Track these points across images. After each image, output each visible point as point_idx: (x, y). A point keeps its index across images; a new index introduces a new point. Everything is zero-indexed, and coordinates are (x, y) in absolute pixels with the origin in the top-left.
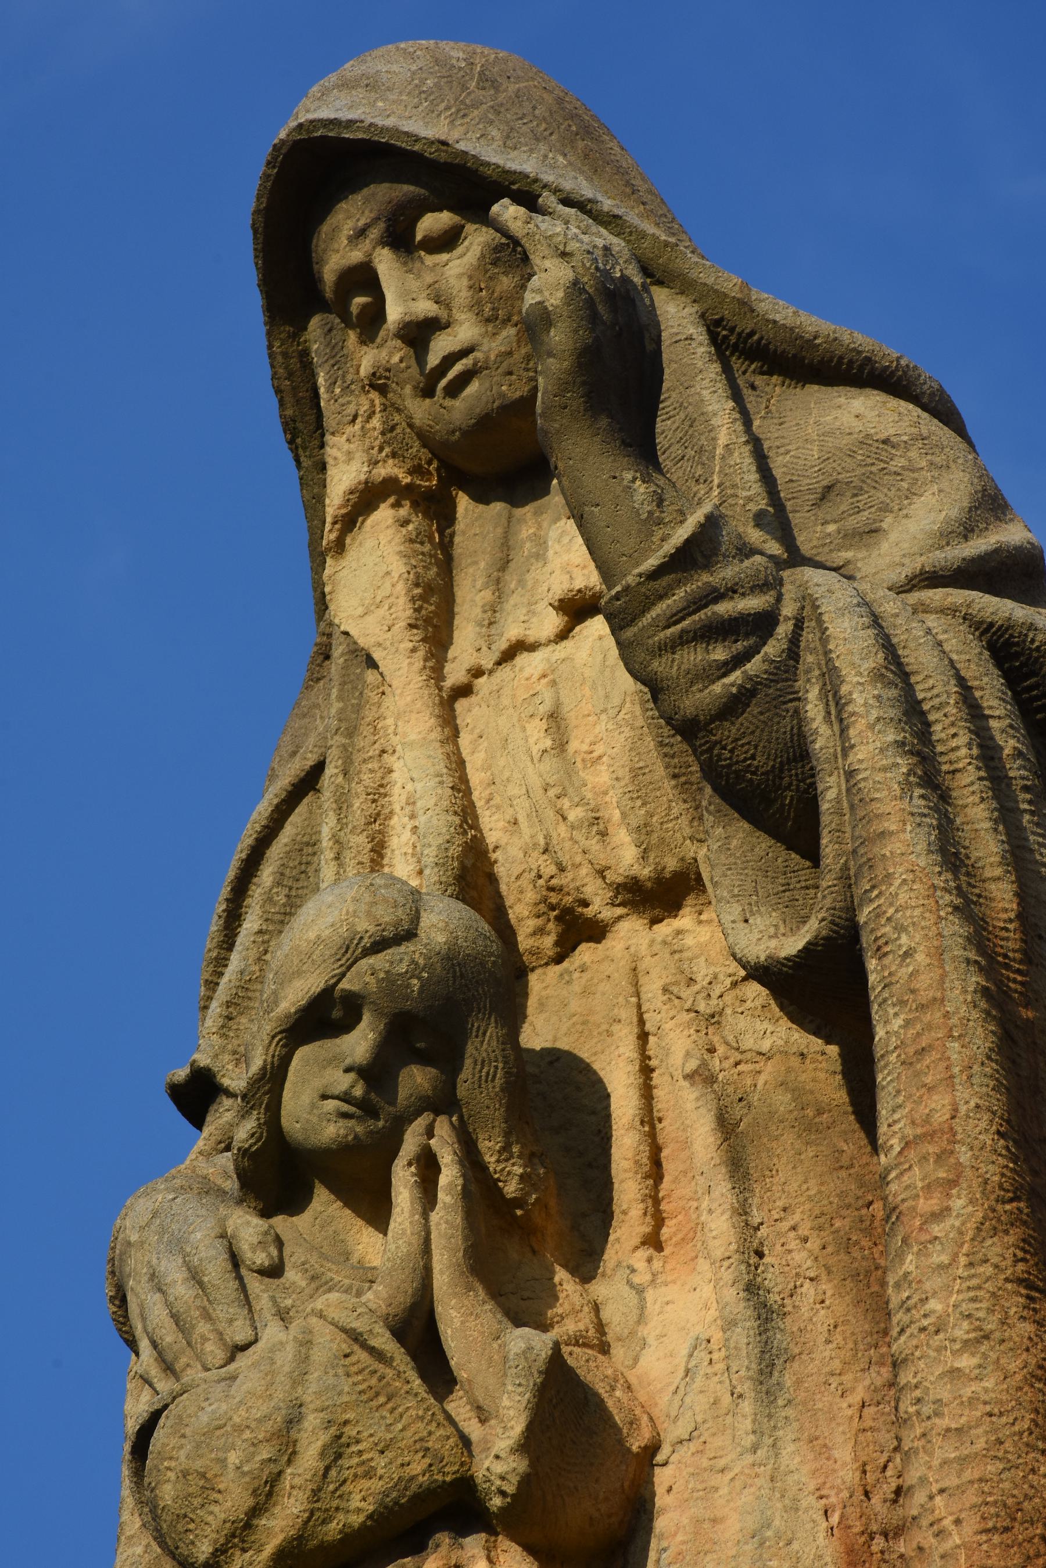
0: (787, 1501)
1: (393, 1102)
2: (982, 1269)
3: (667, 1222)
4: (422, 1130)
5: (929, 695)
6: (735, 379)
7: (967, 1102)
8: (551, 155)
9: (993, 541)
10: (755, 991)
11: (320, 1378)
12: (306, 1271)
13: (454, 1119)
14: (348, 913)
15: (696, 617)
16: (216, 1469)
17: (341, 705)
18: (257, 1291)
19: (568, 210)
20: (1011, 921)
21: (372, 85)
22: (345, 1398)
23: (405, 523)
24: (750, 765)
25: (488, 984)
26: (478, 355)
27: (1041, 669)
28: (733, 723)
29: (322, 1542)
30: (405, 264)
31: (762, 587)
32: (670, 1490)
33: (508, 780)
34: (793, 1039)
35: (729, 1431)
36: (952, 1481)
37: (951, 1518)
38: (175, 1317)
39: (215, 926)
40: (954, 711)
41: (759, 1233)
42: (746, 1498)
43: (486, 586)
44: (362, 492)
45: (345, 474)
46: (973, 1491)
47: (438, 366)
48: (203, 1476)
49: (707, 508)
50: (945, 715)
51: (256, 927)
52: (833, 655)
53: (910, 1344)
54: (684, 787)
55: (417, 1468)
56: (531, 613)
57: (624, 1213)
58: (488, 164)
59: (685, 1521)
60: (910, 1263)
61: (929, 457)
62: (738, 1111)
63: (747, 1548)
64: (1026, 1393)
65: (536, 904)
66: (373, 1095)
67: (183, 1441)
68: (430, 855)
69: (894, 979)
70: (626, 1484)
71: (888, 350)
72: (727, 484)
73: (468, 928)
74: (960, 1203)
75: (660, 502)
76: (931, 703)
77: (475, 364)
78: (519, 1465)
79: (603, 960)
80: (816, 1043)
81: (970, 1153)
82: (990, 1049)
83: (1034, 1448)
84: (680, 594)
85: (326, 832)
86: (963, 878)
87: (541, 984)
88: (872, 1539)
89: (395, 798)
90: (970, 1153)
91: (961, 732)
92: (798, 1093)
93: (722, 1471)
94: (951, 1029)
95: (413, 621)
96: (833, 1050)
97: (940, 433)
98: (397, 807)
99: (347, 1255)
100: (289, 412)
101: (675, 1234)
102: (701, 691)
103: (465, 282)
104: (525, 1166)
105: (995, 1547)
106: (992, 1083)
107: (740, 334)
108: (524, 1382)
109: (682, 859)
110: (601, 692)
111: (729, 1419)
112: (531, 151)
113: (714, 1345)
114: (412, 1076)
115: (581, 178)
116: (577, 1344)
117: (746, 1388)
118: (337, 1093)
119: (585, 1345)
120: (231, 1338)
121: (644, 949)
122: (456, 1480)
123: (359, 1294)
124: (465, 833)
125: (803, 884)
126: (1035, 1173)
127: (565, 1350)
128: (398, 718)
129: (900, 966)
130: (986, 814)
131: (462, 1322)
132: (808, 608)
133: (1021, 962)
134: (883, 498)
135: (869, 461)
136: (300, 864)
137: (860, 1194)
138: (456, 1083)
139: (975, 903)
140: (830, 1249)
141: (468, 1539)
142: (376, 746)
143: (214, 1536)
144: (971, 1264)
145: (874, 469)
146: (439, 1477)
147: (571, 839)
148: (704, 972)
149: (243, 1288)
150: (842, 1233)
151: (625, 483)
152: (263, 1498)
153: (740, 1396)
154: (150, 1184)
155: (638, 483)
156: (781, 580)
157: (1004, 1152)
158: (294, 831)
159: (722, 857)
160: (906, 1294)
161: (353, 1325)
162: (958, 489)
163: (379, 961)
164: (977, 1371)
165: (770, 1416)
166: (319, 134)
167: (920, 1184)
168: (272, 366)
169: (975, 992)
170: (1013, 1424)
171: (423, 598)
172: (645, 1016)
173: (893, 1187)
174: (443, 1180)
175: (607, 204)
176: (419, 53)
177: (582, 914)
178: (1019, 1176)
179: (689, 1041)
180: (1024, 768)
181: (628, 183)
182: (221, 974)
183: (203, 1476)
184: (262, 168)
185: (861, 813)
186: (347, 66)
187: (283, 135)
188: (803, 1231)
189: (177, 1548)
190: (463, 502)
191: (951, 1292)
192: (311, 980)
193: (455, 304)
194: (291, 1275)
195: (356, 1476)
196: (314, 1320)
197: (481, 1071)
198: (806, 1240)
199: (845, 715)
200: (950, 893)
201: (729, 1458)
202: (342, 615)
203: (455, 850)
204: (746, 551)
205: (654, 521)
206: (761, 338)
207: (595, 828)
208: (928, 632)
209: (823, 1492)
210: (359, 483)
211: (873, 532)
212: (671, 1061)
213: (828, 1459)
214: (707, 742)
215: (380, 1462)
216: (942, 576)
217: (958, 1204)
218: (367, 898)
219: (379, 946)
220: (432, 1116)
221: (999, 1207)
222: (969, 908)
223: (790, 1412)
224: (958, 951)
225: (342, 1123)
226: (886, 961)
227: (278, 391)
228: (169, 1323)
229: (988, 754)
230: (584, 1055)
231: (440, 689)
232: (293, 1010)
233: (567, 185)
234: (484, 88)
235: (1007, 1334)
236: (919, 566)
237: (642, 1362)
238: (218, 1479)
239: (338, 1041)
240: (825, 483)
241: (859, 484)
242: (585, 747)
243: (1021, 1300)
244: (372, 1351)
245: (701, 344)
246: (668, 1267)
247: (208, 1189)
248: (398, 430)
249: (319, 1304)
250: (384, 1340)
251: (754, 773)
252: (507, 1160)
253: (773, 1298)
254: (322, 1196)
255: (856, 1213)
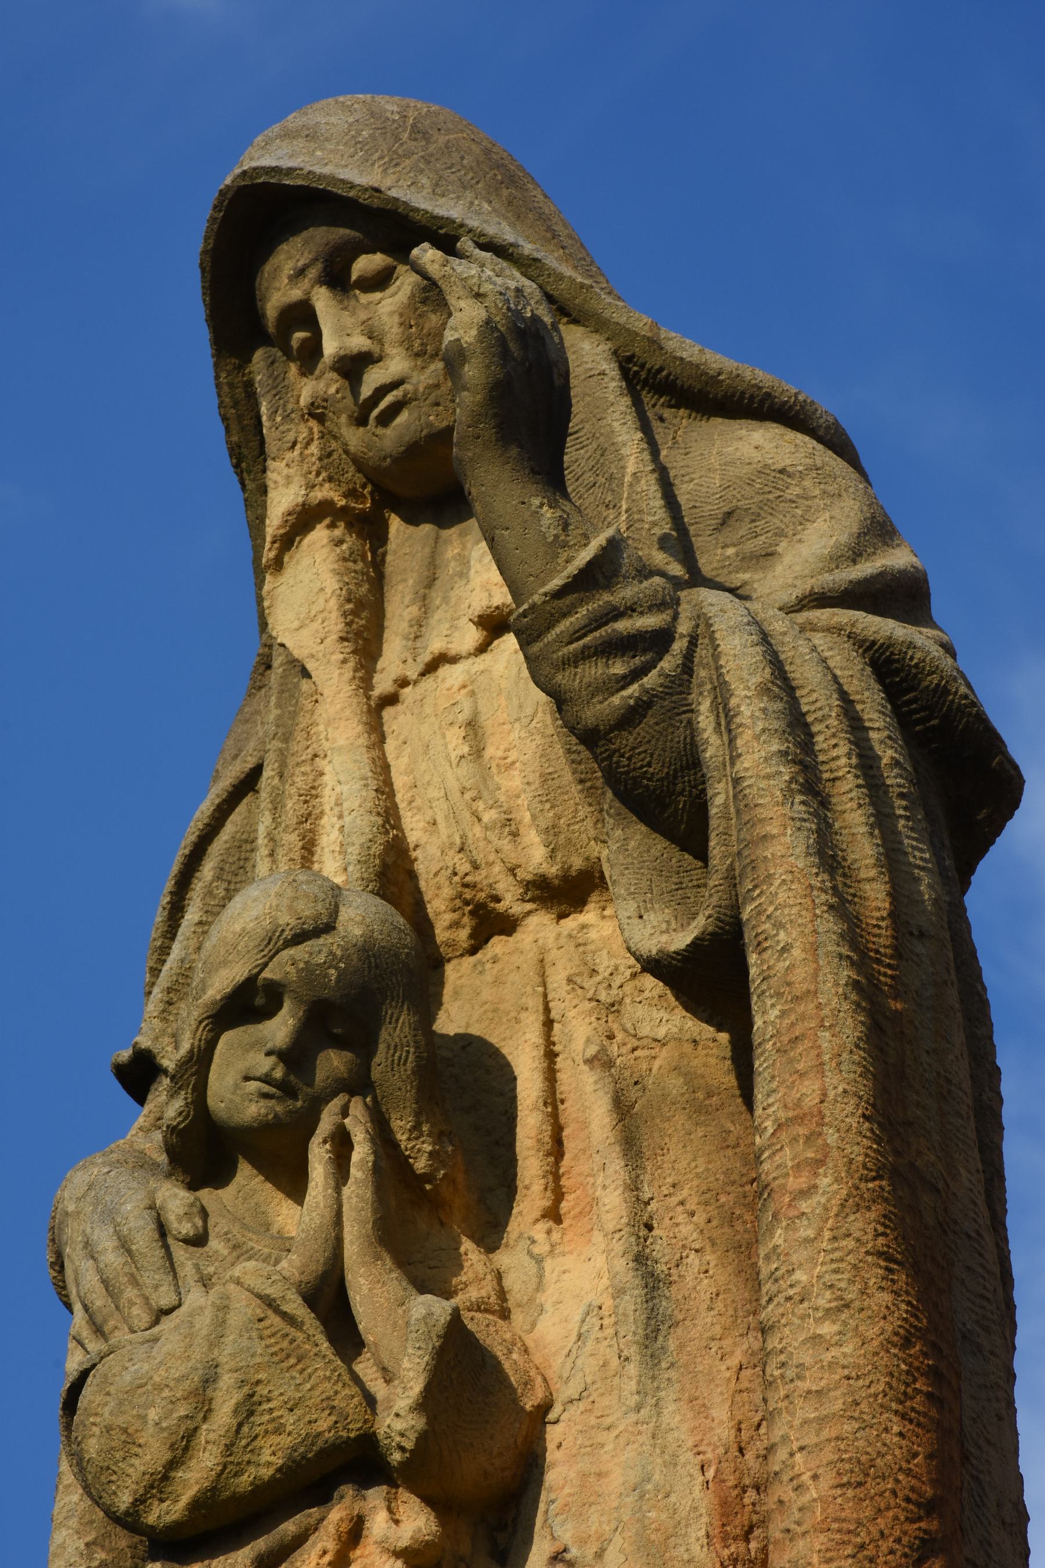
0: (667, 1457)
1: (311, 1084)
2: (845, 1243)
3: (566, 1197)
4: (337, 1110)
5: (813, 708)
6: (645, 412)
7: (835, 1088)
8: (476, 202)
9: (878, 564)
10: (649, 981)
11: (235, 1341)
12: (229, 1240)
13: (368, 1099)
14: (270, 908)
15: (597, 634)
16: (138, 1425)
17: (279, 712)
18: (182, 1259)
19: (483, 253)
20: (883, 919)
21: (312, 135)
22: (258, 1360)
23: (339, 543)
24: (646, 772)
25: (413, 971)
26: (408, 387)
27: (919, 684)
28: (630, 733)
29: (234, 1493)
30: (341, 302)
31: (660, 606)
32: (559, 1446)
33: (428, 783)
34: (687, 1027)
35: (615, 1392)
36: (811, 1439)
37: (809, 1474)
38: (105, 1282)
39: (160, 916)
40: (836, 723)
41: (649, 1208)
42: (629, 1453)
43: (413, 602)
44: (299, 513)
45: (283, 498)
46: (830, 1448)
47: (370, 397)
48: (125, 1431)
49: (610, 532)
50: (827, 727)
51: (196, 918)
52: (724, 671)
53: (776, 1312)
54: (589, 792)
55: (324, 1424)
56: (453, 627)
57: (527, 1188)
58: (418, 210)
59: (572, 1475)
60: (779, 1237)
61: (822, 486)
62: (633, 1093)
63: (627, 1500)
64: (882, 1358)
65: (453, 900)
66: (292, 1077)
67: (108, 1398)
68: (354, 852)
69: (772, 973)
70: (520, 1440)
71: (787, 388)
72: (635, 509)
73: (384, 922)
74: (826, 1181)
75: (565, 527)
76: (814, 716)
77: (405, 396)
78: (415, 1423)
79: (513, 952)
80: (709, 1031)
81: (837, 1135)
82: (859, 1038)
83: (888, 1409)
84: (583, 611)
85: (262, 830)
86: (839, 878)
87: (457, 973)
88: (745, 1492)
89: (325, 799)
90: (837, 1135)
91: (842, 743)
92: (689, 1077)
93: (608, 1429)
94: (823, 1020)
95: (344, 635)
96: (724, 1037)
97: (833, 463)
98: (327, 808)
99: (267, 1226)
100: (235, 439)
101: (573, 1208)
102: (601, 702)
103: (396, 319)
104: (434, 1144)
105: (848, 1500)
106: (859, 1070)
107: (649, 370)
108: (423, 1346)
109: (587, 859)
110: (515, 702)
111: (617, 1380)
112: (458, 198)
113: (605, 1312)
114: (329, 1060)
115: (504, 224)
116: (479, 1310)
117: (632, 1351)
118: (259, 1074)
119: (486, 1311)
120: (157, 1302)
121: (551, 942)
122: (359, 1436)
123: (277, 1262)
124: (387, 832)
125: (695, 883)
126: (897, 1153)
127: (466, 1316)
128: (328, 724)
129: (778, 960)
130: (863, 819)
131: (370, 1290)
132: (702, 627)
133: (891, 957)
134: (778, 524)
135: (767, 489)
136: (239, 859)
137: (745, 1171)
138: (373, 1067)
139: (850, 902)
140: (714, 1223)
141: (371, 1491)
142: (309, 750)
143: (134, 1487)
144: (835, 1238)
145: (771, 497)
146: (344, 1434)
147: (486, 839)
148: (606, 963)
149: (169, 1255)
150: (726, 1208)
151: (533, 508)
152: (180, 1452)
153: (627, 1359)
154: (89, 1159)
155: (545, 508)
156: (679, 599)
157: (868, 1134)
158: (234, 829)
159: (621, 857)
160: (775, 1266)
161: (267, 1292)
162: (848, 516)
163: (299, 952)
164: (838, 1338)
165: (653, 1378)
166: (261, 180)
167: (790, 1164)
168: (219, 396)
169: (846, 985)
170: (869, 1387)
171: (355, 613)
172: (551, 1005)
173: (766, 1166)
174: (356, 1157)
175: (528, 248)
176: (356, 106)
177: (494, 909)
178: (883, 1156)
179: (590, 1028)
180: (901, 776)
181: (549, 229)
182: (163, 962)
183: (125, 1431)
184: (208, 212)
185: (746, 817)
186: (290, 117)
187: (228, 181)
188: (691, 1206)
189: (101, 1498)
190: (395, 524)
191: (816, 1264)
192: (236, 970)
193: (387, 339)
194: (214, 1244)
195: (266, 1432)
196: (232, 1287)
197: (393, 1055)
198: (692, 1214)
199: (733, 727)
200: (826, 892)
201: (615, 1416)
202: (279, 628)
203: (377, 849)
204: (645, 572)
205: (559, 544)
206: (670, 374)
207: (507, 829)
208: (814, 649)
209: (700, 1449)
210: (297, 505)
211: (769, 555)
212: (573, 1047)
213: (706, 1418)
214: (607, 750)
215: (289, 1419)
216: (830, 597)
217: (824, 1181)
218: (290, 893)
219: (299, 938)
220: (347, 1097)
221: (863, 1185)
222: (844, 907)
223: (672, 1374)
224: (831, 945)
225: (263, 1103)
226: (766, 955)
227: (224, 419)
228: (100, 1288)
229: (867, 763)
230: (493, 1040)
231: (369, 698)
232: (218, 997)
233: (491, 230)
234: (416, 140)
235: (866, 1303)
236: (808, 587)
237: (539, 1327)
238: (139, 1434)
239: (260, 1026)
240: (726, 509)
241: (759, 511)
242: (500, 753)
243: (880, 1271)
244: (284, 1315)
245: (613, 379)
246: (566, 1238)
247: (143, 1163)
248: (335, 456)
249: (237, 1271)
250: (295, 1306)
251: (649, 779)
252: (417, 1138)
253: (661, 1268)
254: (245, 1172)
255: (740, 1189)
